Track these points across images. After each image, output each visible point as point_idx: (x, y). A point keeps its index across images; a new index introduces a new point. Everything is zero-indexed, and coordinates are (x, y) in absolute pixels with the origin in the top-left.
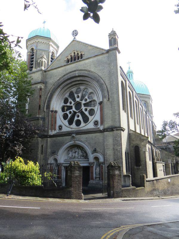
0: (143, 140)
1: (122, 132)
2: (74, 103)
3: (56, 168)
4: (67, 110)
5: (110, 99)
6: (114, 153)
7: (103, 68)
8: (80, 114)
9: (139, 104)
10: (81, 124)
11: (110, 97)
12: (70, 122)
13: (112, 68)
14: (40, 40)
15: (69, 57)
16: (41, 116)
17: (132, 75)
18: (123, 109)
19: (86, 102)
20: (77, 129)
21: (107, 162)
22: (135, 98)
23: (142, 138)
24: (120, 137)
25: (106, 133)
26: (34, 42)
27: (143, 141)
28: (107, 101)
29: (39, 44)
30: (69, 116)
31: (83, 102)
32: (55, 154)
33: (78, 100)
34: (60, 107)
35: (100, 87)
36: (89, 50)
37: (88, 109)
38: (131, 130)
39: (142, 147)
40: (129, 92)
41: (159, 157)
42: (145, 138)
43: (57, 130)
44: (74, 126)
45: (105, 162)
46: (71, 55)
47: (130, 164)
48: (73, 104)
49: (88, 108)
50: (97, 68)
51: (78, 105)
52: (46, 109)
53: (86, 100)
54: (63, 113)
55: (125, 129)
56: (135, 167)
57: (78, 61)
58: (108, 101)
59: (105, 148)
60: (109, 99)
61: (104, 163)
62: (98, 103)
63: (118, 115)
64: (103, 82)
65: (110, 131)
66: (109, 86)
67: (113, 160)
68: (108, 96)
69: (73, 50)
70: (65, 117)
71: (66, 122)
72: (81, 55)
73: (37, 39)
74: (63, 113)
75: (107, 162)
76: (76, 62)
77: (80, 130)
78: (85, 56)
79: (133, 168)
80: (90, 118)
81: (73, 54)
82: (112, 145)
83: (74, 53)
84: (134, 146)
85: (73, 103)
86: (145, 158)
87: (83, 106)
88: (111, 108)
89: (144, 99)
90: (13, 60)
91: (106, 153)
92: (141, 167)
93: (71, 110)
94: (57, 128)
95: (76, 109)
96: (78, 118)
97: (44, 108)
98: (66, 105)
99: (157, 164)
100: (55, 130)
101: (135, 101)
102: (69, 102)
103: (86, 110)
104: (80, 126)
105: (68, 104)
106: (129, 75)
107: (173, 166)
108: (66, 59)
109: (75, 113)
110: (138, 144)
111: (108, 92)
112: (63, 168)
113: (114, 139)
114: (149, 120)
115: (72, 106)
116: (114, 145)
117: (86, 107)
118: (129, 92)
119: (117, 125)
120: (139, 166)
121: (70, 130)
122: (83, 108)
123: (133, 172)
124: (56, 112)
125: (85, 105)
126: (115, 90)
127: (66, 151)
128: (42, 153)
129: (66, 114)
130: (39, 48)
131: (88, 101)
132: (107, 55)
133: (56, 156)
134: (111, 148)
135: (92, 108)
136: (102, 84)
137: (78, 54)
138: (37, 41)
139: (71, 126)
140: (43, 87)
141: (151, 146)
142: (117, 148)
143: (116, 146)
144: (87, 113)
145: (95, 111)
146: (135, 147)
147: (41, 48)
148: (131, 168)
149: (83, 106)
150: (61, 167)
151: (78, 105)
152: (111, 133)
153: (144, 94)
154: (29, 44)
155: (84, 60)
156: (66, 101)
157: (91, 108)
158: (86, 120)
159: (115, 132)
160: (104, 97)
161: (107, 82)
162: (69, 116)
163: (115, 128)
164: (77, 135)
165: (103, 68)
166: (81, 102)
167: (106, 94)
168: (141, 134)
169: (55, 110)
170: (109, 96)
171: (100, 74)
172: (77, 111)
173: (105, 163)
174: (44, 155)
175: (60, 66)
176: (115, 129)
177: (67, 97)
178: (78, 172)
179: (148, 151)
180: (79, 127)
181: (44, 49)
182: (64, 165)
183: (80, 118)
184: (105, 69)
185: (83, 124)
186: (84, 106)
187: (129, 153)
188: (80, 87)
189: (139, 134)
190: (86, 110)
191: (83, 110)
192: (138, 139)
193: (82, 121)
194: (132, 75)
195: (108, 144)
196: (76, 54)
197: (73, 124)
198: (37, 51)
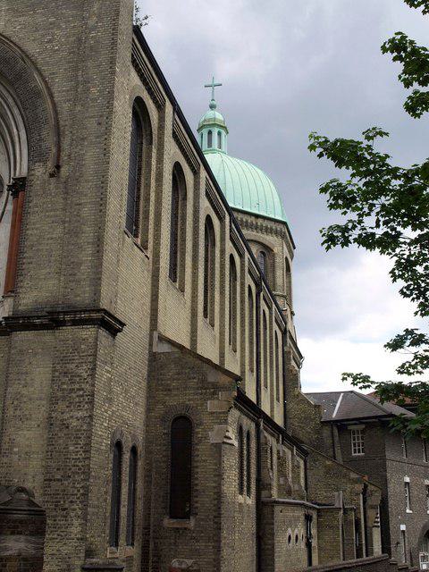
0: (216, 388)
1: (103, 332)
5: (64, 171)
6: (51, 442)
9: (246, 269)
11: (64, 157)
13: (91, 23)
17: (219, 134)
18: (205, 316)
22: (262, 302)
23: (212, 377)
24: (91, 359)
25: (21, 337)
27: (214, 393)
28: (46, 177)
35: (25, 109)
38: (162, 339)
39: (207, 420)
40: (232, 257)
41: (296, 478)
42: (225, 380)
47: (140, 505)
50: (21, 19)
55: (123, 325)
56: (168, 522)
58: (52, 175)
59: (10, 412)
60: (58, 167)
62: (6, 187)
63: (90, 250)
64: (41, 86)
66: (66, 106)
67: (40, 478)
68: (54, 150)
79: (152, 528)
82: (44, 402)
84: (171, 418)
86: (219, 475)
88: (64, 210)
89: (260, 234)
91: (12, 441)
92: (192, 523)
99: (277, 509)
101: (249, 286)
106: (210, 133)
107: (351, 522)
110: (188, 407)
111: (59, 134)
113: (58, 367)
114: (271, 323)
116: (53, 400)
118: (232, 257)
119: (83, 296)
120: (186, 516)
123: (152, 546)
126: (92, 124)
134: (39, 412)
136: (38, 94)
141: (258, 426)
142: (66, 416)
143: (62, 406)
146: (176, 420)
148: (147, 528)
152: (47, 337)
153: (262, 213)
159: (68, 332)
160: (36, 155)
161: (60, 87)
163: (65, 313)
167: (49, 142)
168: (193, 353)
170: (63, 154)
171: (32, 48)
176: (68, 318)
179: (236, 444)
184: (59, 27)
187: (140, 449)
189: (215, 366)
192: (193, 383)
194: (219, 134)
195: (24, 391)
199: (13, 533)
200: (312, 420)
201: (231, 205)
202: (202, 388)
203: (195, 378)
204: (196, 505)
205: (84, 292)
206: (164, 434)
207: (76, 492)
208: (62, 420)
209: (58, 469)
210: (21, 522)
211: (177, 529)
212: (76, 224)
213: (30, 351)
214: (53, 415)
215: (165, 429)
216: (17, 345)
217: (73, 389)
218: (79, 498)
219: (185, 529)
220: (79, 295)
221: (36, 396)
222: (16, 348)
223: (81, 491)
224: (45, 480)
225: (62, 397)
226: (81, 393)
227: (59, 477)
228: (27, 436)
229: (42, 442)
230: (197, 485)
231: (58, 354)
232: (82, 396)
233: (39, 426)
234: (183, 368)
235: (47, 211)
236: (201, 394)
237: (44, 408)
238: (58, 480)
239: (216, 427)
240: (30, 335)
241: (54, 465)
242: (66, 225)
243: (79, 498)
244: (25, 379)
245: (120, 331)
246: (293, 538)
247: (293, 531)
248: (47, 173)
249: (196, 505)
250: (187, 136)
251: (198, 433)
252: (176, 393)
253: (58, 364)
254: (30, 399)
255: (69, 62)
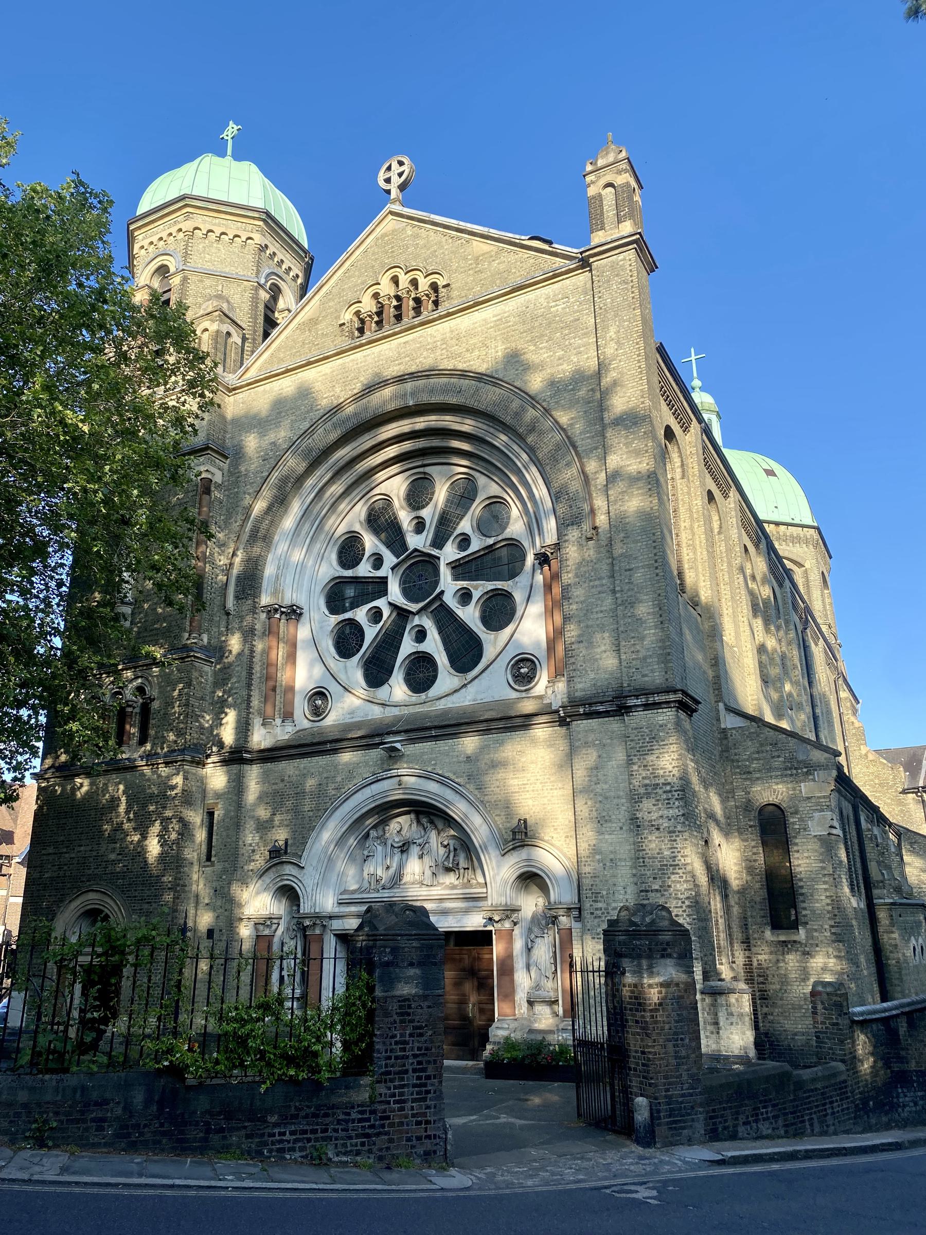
2: (395, 561)
3: (290, 945)
4: (355, 605)
7: (560, 353)
8: (428, 624)
10: (435, 677)
12: (377, 673)
14: (203, 221)
15: (368, 305)
16: (205, 638)
19: (464, 554)
20: (412, 710)
21: (600, 905)
26: (173, 230)
27: (808, 773)
29: (198, 245)
30: (371, 633)
31: (450, 552)
32: (284, 858)
33: (414, 541)
34: (319, 588)
36: (477, 259)
37: (476, 595)
43: (302, 719)
44: (397, 688)
45: (587, 905)
46: (376, 296)
48: (393, 569)
49: (476, 588)
51: (420, 572)
52: (237, 598)
53: (464, 541)
54: (334, 619)
55: (697, 702)
57: (417, 321)
61: (580, 909)
65: (607, 714)
69: (389, 262)
70: (347, 640)
71: (353, 671)
72: (434, 287)
73: (188, 216)
74: (334, 619)
75: (600, 905)
76: (441, 318)
77: (446, 712)
78: (455, 294)
80: (493, 643)
81: (386, 288)
83: (395, 280)
85: (390, 559)
87: (449, 578)
90: (665, 891)
92: (802, 934)
93: (381, 603)
94: (301, 708)
95: (407, 592)
96: (423, 647)
97: (224, 596)
98: (349, 573)
100: (288, 716)
102: (367, 554)
103: (465, 597)
104: (434, 692)
105: (364, 569)
108: (348, 316)
109: (402, 615)
112: (330, 945)
115: (384, 581)
117: (464, 584)
121: (376, 712)
122: (448, 585)
124: (294, 611)
125: (460, 569)
127: (352, 841)
128: (209, 858)
129: (352, 622)
130: (196, 261)
131: (476, 545)
132: (582, 278)
133: (288, 869)
135: (499, 584)
137: (414, 283)
138: (187, 226)
139: (382, 693)
140: (218, 478)
144: (470, 615)
145: (480, 656)
147: (208, 266)
149: (445, 573)
150: (320, 939)
151: (420, 572)
154: (145, 243)
155: (449, 315)
156: (350, 550)
157: (490, 585)
158: (466, 652)
159: (639, 718)
162: (371, 633)
163: (637, 697)
164: (413, 741)
165: (560, 353)
166: (435, 552)
169: (287, 602)
172: (414, 607)
173: (586, 914)
174: (218, 867)
175: (314, 354)
177: (357, 528)
178: (418, 971)
180: (423, 696)
181: (227, 270)
182: (336, 925)
183: (434, 645)
185: (446, 679)
186: (456, 578)
188: (428, 470)
190: (465, 597)
191: (450, 600)
193: (442, 659)
196: (404, 280)
197: (392, 681)
198: (185, 279)
199: (663, 956)
200: (891, 787)
201: (762, 516)
202: (791, 769)
203: (779, 757)
204: (804, 912)
205: (652, 671)
206: (751, 827)
207: (680, 904)
208: (650, 821)
209: (654, 878)
210: (668, 944)
211: (784, 942)
212: (629, 593)
213: (597, 742)
214: (638, 816)
215: (750, 820)
216: (580, 736)
217: (658, 785)
218: (684, 911)
219: (795, 942)
220: (646, 675)
221: (612, 794)
222: (580, 740)
223: (687, 903)
224: (642, 891)
225: (644, 794)
226: (668, 788)
227: (657, 887)
228: (610, 841)
229: (628, 847)
230: (802, 887)
231: (633, 744)
232: (670, 791)
233: (621, 828)
234: (762, 745)
235: (591, 581)
236: (791, 775)
237: (624, 808)
238: (657, 891)
239: (816, 814)
240: (593, 723)
241: (648, 873)
242: (618, 595)
243: (684, 911)
244: (597, 776)
245: (695, 710)
246: (918, 950)
247: (917, 941)
248: (584, 538)
249: (804, 912)
250: (715, 456)
251: (794, 823)
252: (758, 775)
253: (635, 755)
254: (606, 798)
255: (589, 403)
